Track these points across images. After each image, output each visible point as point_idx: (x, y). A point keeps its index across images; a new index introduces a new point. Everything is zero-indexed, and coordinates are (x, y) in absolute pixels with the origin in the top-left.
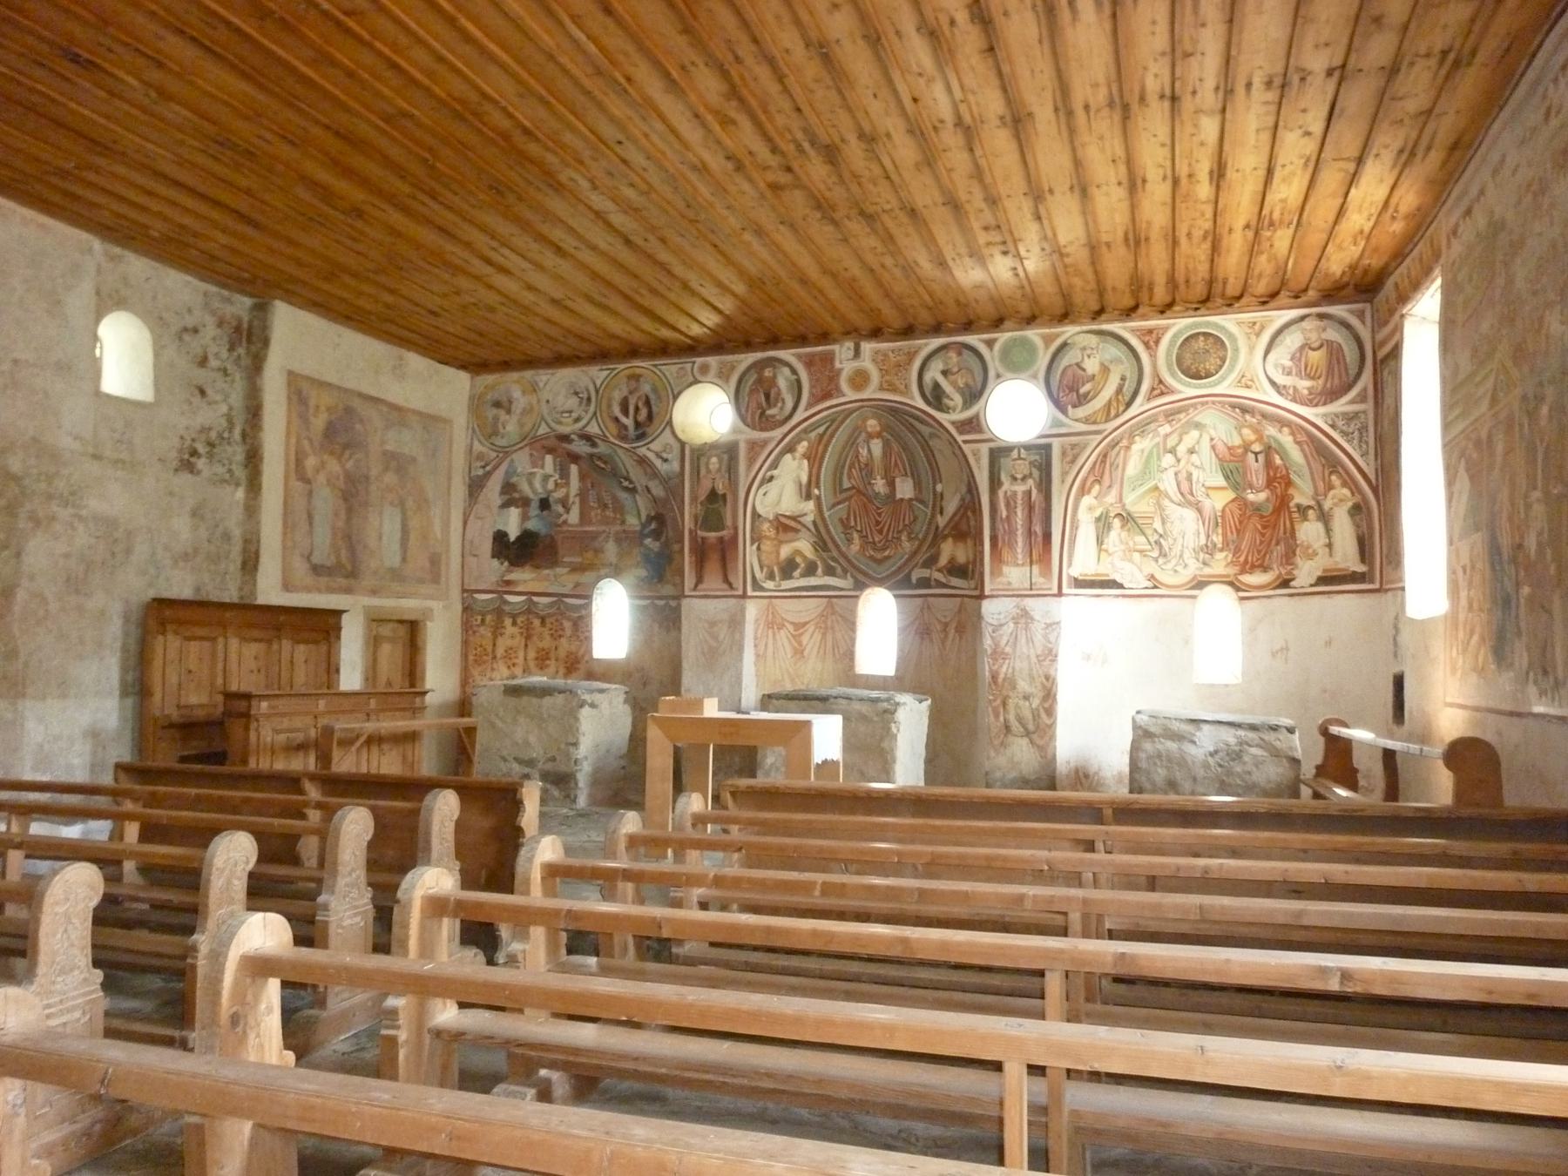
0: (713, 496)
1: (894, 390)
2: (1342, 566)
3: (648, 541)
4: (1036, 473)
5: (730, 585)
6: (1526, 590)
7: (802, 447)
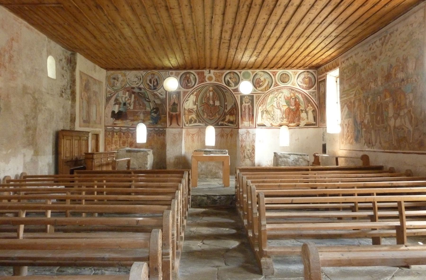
0: (174, 104)
1: (219, 81)
4: (250, 101)
5: (179, 125)
6: (364, 129)
7: (195, 93)
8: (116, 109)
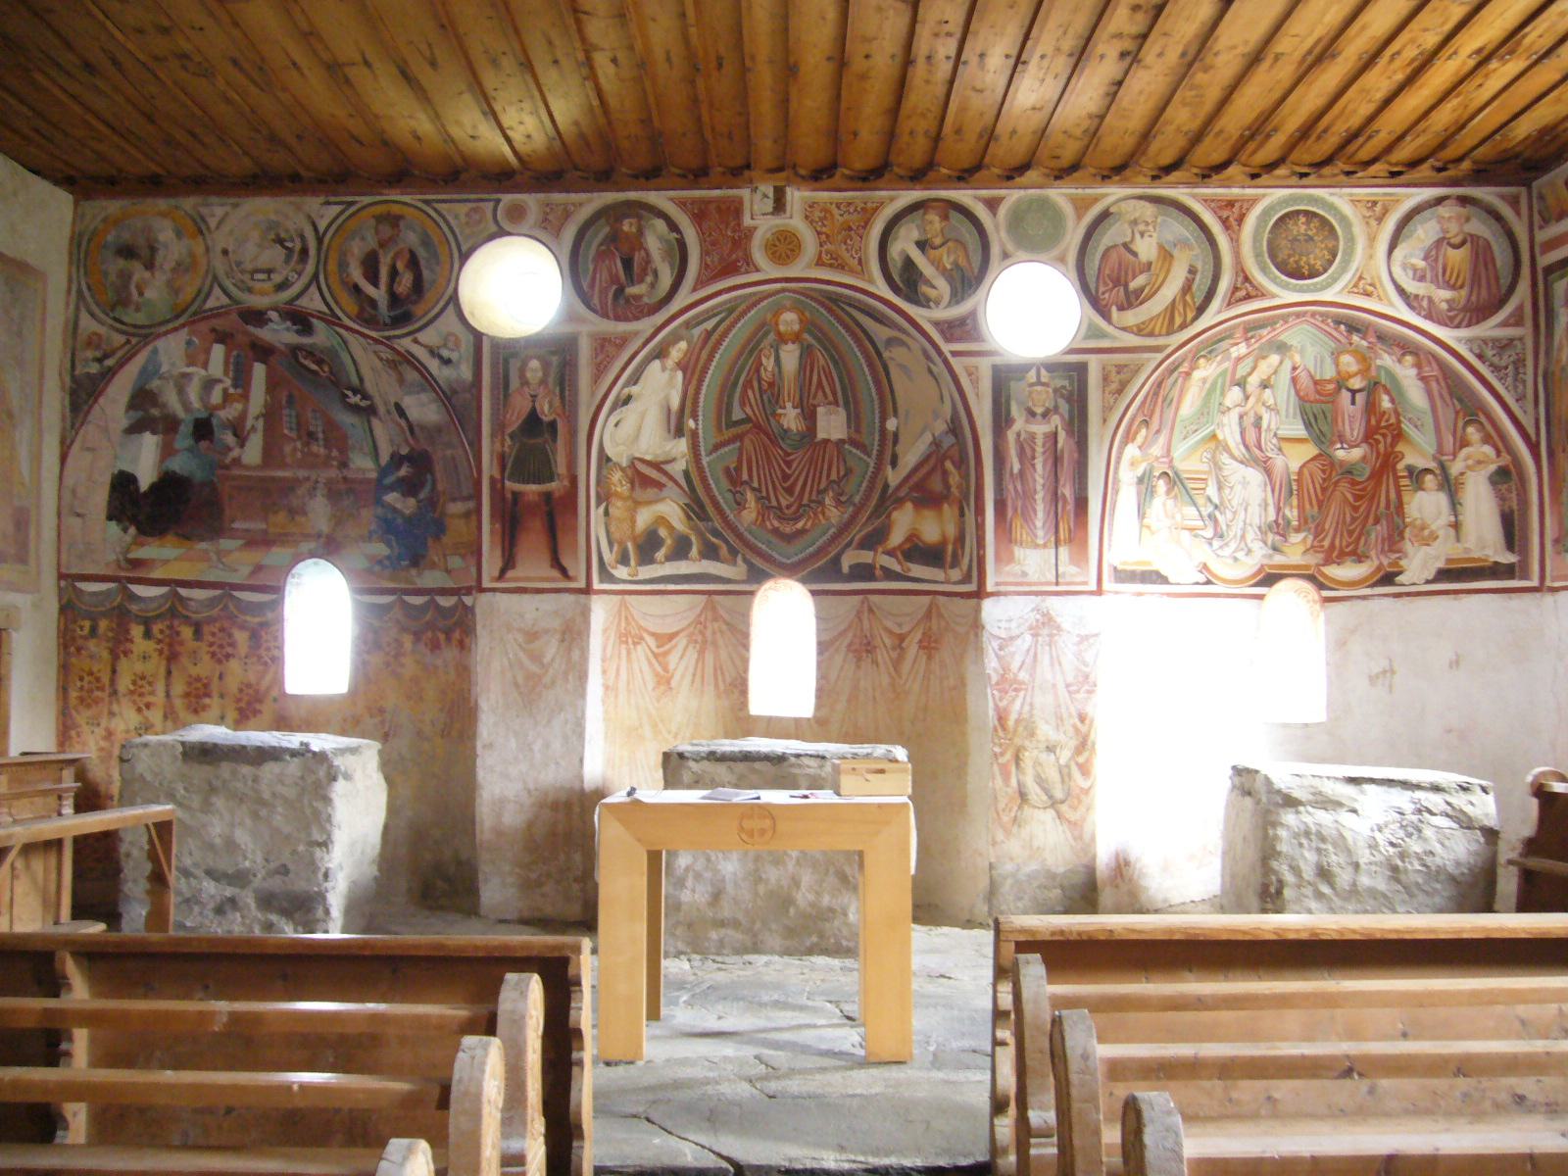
0: (533, 423)
1: (841, 267)
2: (1476, 555)
3: (392, 498)
4: (1064, 407)
5: (564, 572)
8: (145, 461)
